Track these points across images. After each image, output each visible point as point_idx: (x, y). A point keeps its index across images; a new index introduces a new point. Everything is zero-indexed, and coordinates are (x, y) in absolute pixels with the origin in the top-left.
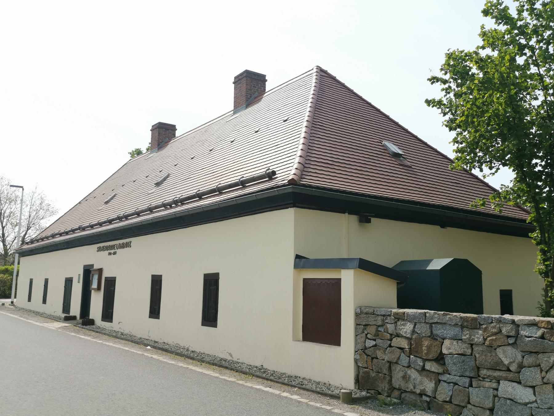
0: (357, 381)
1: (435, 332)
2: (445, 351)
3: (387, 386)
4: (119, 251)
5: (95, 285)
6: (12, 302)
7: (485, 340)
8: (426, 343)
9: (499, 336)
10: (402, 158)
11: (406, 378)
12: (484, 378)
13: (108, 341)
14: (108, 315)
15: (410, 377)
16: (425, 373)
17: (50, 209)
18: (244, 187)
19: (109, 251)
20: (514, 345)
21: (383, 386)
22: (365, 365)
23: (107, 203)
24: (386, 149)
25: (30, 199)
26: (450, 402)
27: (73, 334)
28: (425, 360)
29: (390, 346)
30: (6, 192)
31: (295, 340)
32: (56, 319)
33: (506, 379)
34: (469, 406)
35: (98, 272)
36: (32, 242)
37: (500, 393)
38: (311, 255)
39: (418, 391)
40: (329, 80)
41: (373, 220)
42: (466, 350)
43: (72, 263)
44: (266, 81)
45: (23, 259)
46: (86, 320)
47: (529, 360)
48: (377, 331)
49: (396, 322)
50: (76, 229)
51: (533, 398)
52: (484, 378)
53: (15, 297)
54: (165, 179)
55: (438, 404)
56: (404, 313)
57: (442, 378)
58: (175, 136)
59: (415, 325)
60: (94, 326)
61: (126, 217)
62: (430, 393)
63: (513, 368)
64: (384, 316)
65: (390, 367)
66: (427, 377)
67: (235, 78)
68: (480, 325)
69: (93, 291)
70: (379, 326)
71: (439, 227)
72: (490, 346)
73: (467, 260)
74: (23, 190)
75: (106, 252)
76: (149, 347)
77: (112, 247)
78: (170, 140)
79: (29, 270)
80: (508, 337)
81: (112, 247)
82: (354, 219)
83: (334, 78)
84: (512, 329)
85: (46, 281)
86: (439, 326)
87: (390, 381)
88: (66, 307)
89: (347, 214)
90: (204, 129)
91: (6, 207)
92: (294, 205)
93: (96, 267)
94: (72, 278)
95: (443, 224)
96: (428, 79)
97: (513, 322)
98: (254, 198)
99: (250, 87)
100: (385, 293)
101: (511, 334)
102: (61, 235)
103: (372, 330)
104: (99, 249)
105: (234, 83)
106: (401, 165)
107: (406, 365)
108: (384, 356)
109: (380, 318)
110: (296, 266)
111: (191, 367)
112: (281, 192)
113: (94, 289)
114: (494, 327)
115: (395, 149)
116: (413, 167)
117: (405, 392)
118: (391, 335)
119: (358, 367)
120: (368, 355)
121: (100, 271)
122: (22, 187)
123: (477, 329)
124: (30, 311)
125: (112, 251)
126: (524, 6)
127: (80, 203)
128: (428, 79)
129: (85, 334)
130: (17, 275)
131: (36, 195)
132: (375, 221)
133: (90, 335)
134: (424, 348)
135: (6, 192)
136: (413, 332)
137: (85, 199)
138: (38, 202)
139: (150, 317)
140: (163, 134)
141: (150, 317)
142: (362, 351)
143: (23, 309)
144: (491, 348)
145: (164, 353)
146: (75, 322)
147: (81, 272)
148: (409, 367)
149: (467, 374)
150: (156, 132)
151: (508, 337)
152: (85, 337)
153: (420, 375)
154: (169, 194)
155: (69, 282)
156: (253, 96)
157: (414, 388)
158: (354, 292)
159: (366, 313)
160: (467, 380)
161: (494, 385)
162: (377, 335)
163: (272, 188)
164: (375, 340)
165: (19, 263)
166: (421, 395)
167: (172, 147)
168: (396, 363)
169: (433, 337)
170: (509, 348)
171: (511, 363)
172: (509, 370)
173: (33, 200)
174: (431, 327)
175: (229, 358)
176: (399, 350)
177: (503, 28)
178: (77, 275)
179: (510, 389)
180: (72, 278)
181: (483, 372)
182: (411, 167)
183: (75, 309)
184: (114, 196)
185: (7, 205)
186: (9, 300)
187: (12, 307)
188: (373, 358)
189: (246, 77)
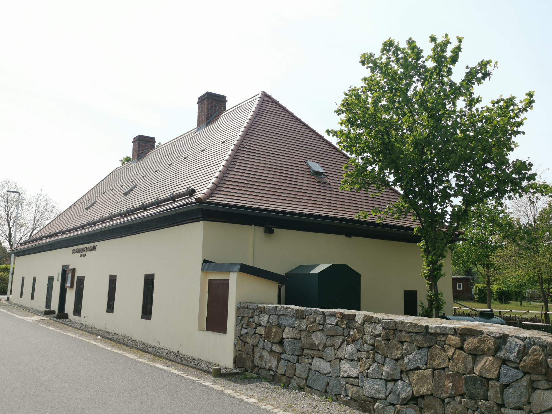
0: (235, 362)
1: (281, 322)
2: (285, 336)
3: (251, 364)
4: (88, 253)
5: (68, 284)
6: (8, 298)
7: (307, 327)
8: (274, 330)
9: (314, 324)
10: (323, 176)
11: (261, 357)
12: (305, 356)
13: (69, 332)
14: (77, 311)
15: (263, 356)
16: (272, 353)
17: (54, 211)
18: (175, 201)
19: (81, 253)
20: (322, 330)
21: (249, 364)
22: (240, 349)
23: (87, 209)
24: (309, 167)
25: (35, 201)
26: (284, 375)
27: (45, 326)
28: (273, 343)
29: (255, 333)
31: (200, 329)
32: (36, 312)
33: (317, 357)
34: (295, 377)
35: (71, 272)
36: (25, 243)
37: (313, 367)
38: (218, 260)
39: (268, 368)
40: (271, 105)
41: (276, 230)
42: (297, 335)
43: (50, 264)
44: (227, 101)
45: (18, 259)
46: (62, 315)
47: (330, 341)
48: (249, 321)
49: (259, 315)
50: (58, 233)
51: (329, 370)
52: (305, 356)
53: (11, 294)
54: (132, 190)
55: (278, 377)
56: (264, 307)
57: (283, 356)
59: (269, 316)
60: (67, 320)
61: (94, 223)
62: (274, 369)
63: (320, 348)
64: (254, 309)
65: (253, 349)
66: (274, 356)
67: (199, 98)
68: (306, 316)
69: (68, 289)
70: (250, 318)
71: (344, 237)
72: (309, 332)
73: (345, 267)
74: (19, 195)
75: (79, 254)
76: (99, 337)
77: (83, 250)
78: (149, 151)
79: (23, 269)
80: (320, 324)
81: (83, 250)
82: (260, 230)
83: (276, 103)
84: (321, 318)
85: (35, 279)
86: (284, 317)
87: (253, 360)
88: (48, 303)
89: (253, 226)
90: (174, 144)
92: (204, 219)
93: (71, 267)
94: (53, 277)
95: (349, 234)
96: (336, 112)
97: (323, 313)
98: (175, 213)
99: (212, 106)
100: (266, 294)
101: (320, 322)
102: (46, 237)
103: (245, 320)
104: (75, 251)
105: (198, 103)
106: (319, 182)
107: (262, 347)
108: (251, 341)
109: (251, 311)
110: (203, 269)
111: (121, 352)
112: (191, 208)
113: (68, 287)
114: (312, 317)
115: (317, 167)
116: (331, 184)
117: (261, 368)
118: (256, 324)
119: (236, 350)
120: (242, 341)
121: (74, 271)
122: (18, 192)
123: (303, 319)
124: (21, 306)
125: (83, 254)
126: (390, 58)
127: (70, 208)
128: (336, 112)
129: (55, 326)
130: (13, 274)
131: (41, 197)
133: (58, 327)
134: (273, 334)
136: (268, 322)
137: (74, 204)
138: (43, 204)
139: (107, 312)
140: (144, 145)
141: (107, 312)
142: (239, 337)
143: (16, 304)
144: (310, 333)
145: (109, 341)
146: (52, 316)
147: (60, 272)
148: (263, 349)
149: (296, 353)
150: (137, 144)
151: (320, 324)
152: (55, 329)
153: (270, 355)
154: (135, 201)
155: (51, 280)
156: (214, 115)
157: (266, 365)
158: (238, 289)
159: (243, 308)
160: (296, 358)
161: (310, 361)
162: (248, 324)
163: (187, 204)
164: (247, 329)
165: (14, 263)
166: (269, 370)
167: (151, 157)
168: (257, 346)
169: (279, 325)
170: (320, 333)
171: (319, 344)
172: (319, 350)
173: (39, 202)
174: (279, 318)
175: (158, 345)
176: (259, 336)
177: (430, 64)
178: (57, 274)
179: (318, 364)
180: (53, 277)
181: (305, 351)
182: (329, 184)
183: (55, 306)
184: (94, 203)
185: (14, 206)
186: (6, 297)
187: (7, 303)
188: (245, 343)
189: (207, 98)
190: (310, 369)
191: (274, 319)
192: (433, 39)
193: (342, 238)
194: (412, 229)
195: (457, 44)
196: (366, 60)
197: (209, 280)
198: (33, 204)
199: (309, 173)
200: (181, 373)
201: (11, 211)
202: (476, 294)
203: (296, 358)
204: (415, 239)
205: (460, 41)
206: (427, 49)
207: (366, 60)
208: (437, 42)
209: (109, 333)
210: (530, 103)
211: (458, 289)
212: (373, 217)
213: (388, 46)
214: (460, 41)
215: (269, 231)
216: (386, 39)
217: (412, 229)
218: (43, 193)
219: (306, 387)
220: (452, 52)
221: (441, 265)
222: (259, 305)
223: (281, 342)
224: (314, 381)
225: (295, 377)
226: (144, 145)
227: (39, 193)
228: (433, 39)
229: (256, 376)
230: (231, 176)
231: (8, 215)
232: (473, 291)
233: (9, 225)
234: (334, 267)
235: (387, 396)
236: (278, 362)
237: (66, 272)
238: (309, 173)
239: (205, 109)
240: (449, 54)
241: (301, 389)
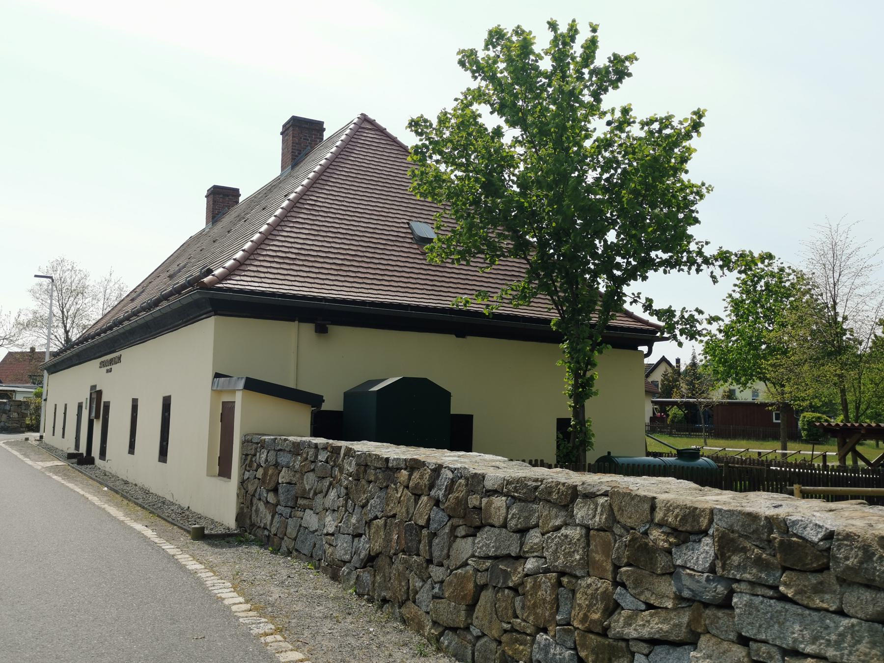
1: (279, 460)
14: (103, 454)
20: (313, 470)
25: (102, 290)
30: (69, 281)
31: (210, 474)
44: (324, 130)
58: (237, 202)
67: (284, 126)
71: (454, 336)
73: (425, 381)
82: (308, 329)
86: (282, 453)
91: (70, 303)
104: (103, 364)
105: (282, 134)
122: (51, 277)
125: (109, 368)
131: (111, 284)
132: (334, 329)
135: (69, 281)
136: (266, 460)
140: (221, 199)
142: (242, 483)
155: (80, 406)
169: (276, 465)
171: (310, 489)
173: (108, 291)
177: (546, 64)
183: (83, 449)
185: (72, 299)
190: (300, 526)
191: (272, 458)
192: (553, 26)
193: (449, 340)
194: (549, 321)
195: (590, 35)
196: (468, 60)
197: (223, 403)
198: (101, 296)
199: (410, 241)
200: (149, 533)
201: (68, 306)
202: (804, 430)
203: (288, 510)
204: (555, 338)
205: (594, 30)
206: (542, 41)
207: (468, 60)
208: (559, 32)
209: (126, 483)
210: (696, 126)
211: (774, 421)
212: (477, 305)
213: (496, 36)
214: (594, 30)
215: (321, 330)
216: (492, 26)
217: (548, 321)
218: (114, 278)
219: (294, 551)
220: (582, 47)
221: (592, 378)
222: (291, 438)
223: (275, 490)
224: (303, 542)
225: (286, 538)
226: (221, 199)
227: (108, 277)
228: (553, 26)
229: (253, 537)
230: (271, 248)
231: (63, 312)
232: (800, 424)
233: (65, 327)
234: (404, 380)
235: (352, 557)
236: (273, 517)
237: (96, 395)
238: (410, 241)
239: (290, 143)
240: (577, 49)
241: (289, 553)
